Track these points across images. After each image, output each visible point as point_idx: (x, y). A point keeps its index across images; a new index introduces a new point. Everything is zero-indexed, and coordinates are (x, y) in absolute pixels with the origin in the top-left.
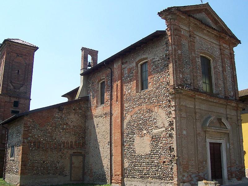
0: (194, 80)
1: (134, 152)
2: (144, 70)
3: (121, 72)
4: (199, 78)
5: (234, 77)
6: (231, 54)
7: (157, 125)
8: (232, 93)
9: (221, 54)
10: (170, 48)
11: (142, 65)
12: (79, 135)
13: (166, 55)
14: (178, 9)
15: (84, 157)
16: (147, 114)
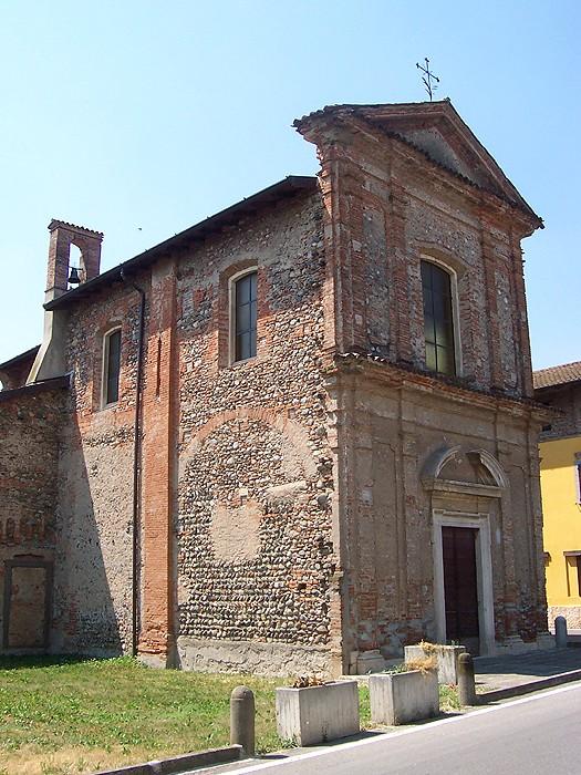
0: (398, 334)
1: (210, 554)
2: (246, 299)
3: (174, 302)
4: (414, 327)
5: (519, 330)
6: (512, 257)
7: (281, 470)
8: (514, 378)
9: (483, 257)
10: (328, 232)
11: (238, 282)
12: (35, 501)
13: (315, 255)
14: (356, 111)
15: (50, 568)
16: (252, 436)
